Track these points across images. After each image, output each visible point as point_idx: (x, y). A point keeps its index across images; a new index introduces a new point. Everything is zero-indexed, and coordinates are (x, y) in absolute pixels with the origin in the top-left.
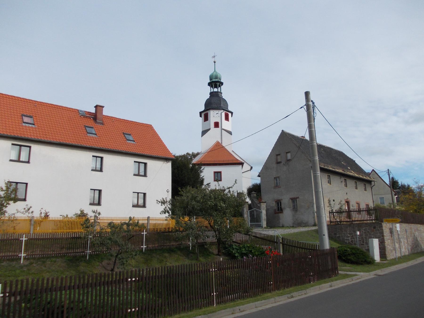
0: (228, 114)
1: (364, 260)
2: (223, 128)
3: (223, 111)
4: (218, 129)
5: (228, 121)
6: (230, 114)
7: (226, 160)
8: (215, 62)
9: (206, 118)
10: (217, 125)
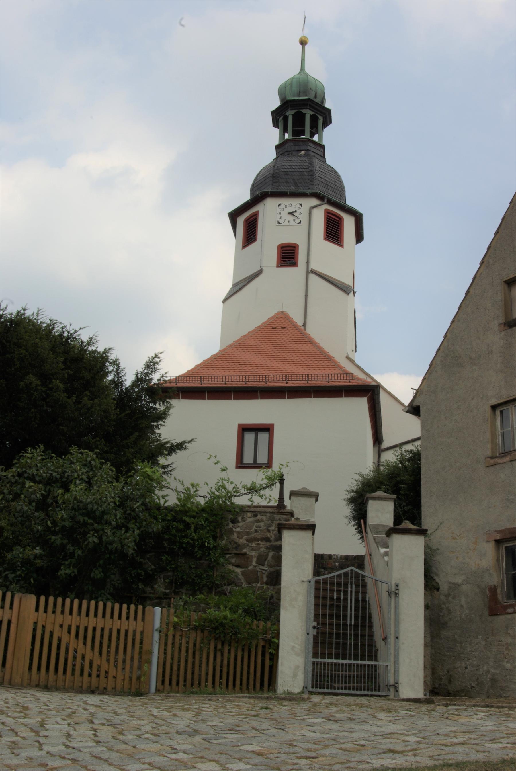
0: (340, 219)
1: (259, 517)
2: (313, 266)
3: (314, 202)
4: (294, 275)
5: (341, 245)
6: (348, 224)
7: (297, 374)
8: (303, 43)
9: (250, 235)
10: (288, 255)
